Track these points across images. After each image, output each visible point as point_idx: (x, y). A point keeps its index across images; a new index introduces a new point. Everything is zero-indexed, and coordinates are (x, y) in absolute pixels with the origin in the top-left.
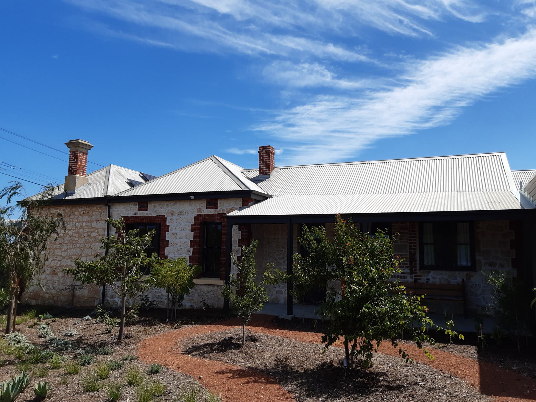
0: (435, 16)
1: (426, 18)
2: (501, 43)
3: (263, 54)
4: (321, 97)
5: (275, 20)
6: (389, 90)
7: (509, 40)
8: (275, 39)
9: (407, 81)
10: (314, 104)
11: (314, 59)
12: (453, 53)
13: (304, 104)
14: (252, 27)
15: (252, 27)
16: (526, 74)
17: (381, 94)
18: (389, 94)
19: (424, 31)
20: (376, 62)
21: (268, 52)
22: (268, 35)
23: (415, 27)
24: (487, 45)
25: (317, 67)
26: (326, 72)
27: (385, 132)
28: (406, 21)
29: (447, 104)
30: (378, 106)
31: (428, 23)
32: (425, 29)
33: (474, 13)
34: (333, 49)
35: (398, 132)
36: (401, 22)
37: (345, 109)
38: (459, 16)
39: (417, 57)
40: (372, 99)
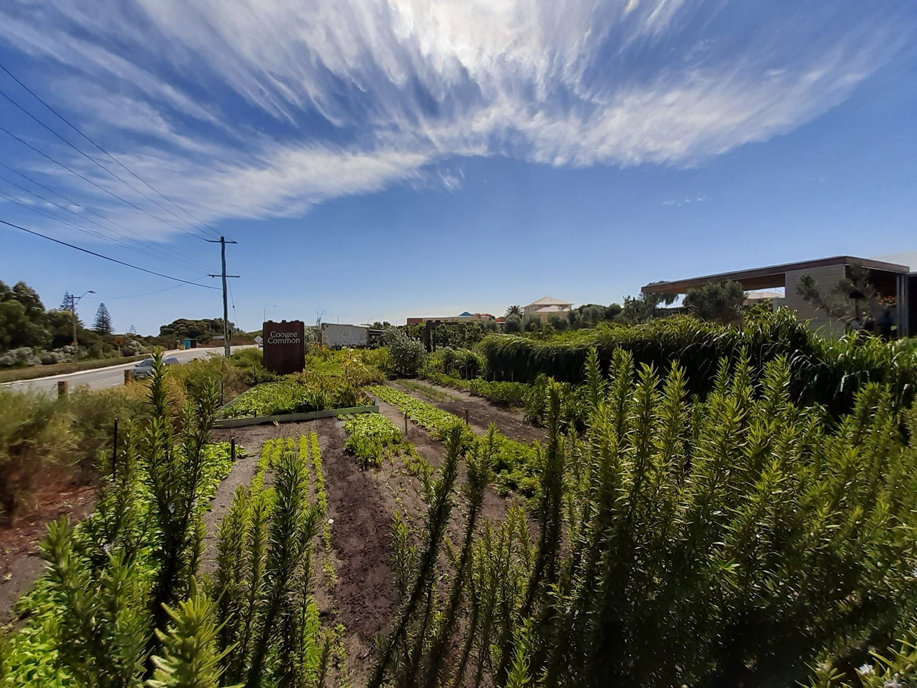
0: (299, 103)
1: (290, 101)
2: (355, 153)
3: (53, 61)
4: (148, 149)
5: (81, 19)
6: (242, 167)
7: (360, 154)
8: (75, 44)
9: (264, 162)
10: (139, 157)
11: (141, 95)
12: (311, 148)
13: (124, 153)
14: (39, 15)
15: (39, 15)
16: (564, 161)
17: (233, 169)
18: (242, 171)
19: (286, 114)
20: (228, 128)
21: (62, 59)
22: (64, 35)
23: (277, 105)
24: (343, 151)
25: (145, 108)
26: (160, 120)
27: (235, 212)
28: (267, 93)
29: (301, 198)
30: (228, 182)
31: (291, 107)
32: (287, 113)
33: (335, 115)
34: (168, 91)
35: (250, 215)
36: (261, 92)
37: (184, 174)
38: (321, 111)
39: (277, 139)
40: (220, 171)
